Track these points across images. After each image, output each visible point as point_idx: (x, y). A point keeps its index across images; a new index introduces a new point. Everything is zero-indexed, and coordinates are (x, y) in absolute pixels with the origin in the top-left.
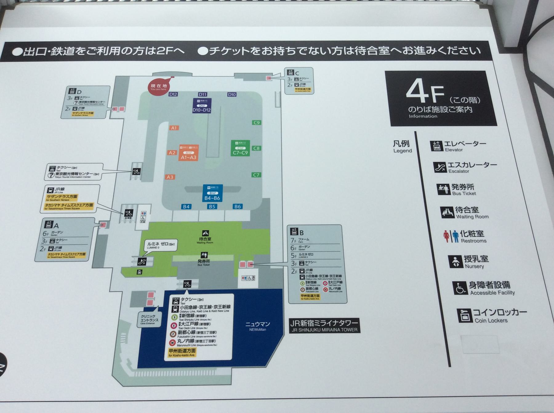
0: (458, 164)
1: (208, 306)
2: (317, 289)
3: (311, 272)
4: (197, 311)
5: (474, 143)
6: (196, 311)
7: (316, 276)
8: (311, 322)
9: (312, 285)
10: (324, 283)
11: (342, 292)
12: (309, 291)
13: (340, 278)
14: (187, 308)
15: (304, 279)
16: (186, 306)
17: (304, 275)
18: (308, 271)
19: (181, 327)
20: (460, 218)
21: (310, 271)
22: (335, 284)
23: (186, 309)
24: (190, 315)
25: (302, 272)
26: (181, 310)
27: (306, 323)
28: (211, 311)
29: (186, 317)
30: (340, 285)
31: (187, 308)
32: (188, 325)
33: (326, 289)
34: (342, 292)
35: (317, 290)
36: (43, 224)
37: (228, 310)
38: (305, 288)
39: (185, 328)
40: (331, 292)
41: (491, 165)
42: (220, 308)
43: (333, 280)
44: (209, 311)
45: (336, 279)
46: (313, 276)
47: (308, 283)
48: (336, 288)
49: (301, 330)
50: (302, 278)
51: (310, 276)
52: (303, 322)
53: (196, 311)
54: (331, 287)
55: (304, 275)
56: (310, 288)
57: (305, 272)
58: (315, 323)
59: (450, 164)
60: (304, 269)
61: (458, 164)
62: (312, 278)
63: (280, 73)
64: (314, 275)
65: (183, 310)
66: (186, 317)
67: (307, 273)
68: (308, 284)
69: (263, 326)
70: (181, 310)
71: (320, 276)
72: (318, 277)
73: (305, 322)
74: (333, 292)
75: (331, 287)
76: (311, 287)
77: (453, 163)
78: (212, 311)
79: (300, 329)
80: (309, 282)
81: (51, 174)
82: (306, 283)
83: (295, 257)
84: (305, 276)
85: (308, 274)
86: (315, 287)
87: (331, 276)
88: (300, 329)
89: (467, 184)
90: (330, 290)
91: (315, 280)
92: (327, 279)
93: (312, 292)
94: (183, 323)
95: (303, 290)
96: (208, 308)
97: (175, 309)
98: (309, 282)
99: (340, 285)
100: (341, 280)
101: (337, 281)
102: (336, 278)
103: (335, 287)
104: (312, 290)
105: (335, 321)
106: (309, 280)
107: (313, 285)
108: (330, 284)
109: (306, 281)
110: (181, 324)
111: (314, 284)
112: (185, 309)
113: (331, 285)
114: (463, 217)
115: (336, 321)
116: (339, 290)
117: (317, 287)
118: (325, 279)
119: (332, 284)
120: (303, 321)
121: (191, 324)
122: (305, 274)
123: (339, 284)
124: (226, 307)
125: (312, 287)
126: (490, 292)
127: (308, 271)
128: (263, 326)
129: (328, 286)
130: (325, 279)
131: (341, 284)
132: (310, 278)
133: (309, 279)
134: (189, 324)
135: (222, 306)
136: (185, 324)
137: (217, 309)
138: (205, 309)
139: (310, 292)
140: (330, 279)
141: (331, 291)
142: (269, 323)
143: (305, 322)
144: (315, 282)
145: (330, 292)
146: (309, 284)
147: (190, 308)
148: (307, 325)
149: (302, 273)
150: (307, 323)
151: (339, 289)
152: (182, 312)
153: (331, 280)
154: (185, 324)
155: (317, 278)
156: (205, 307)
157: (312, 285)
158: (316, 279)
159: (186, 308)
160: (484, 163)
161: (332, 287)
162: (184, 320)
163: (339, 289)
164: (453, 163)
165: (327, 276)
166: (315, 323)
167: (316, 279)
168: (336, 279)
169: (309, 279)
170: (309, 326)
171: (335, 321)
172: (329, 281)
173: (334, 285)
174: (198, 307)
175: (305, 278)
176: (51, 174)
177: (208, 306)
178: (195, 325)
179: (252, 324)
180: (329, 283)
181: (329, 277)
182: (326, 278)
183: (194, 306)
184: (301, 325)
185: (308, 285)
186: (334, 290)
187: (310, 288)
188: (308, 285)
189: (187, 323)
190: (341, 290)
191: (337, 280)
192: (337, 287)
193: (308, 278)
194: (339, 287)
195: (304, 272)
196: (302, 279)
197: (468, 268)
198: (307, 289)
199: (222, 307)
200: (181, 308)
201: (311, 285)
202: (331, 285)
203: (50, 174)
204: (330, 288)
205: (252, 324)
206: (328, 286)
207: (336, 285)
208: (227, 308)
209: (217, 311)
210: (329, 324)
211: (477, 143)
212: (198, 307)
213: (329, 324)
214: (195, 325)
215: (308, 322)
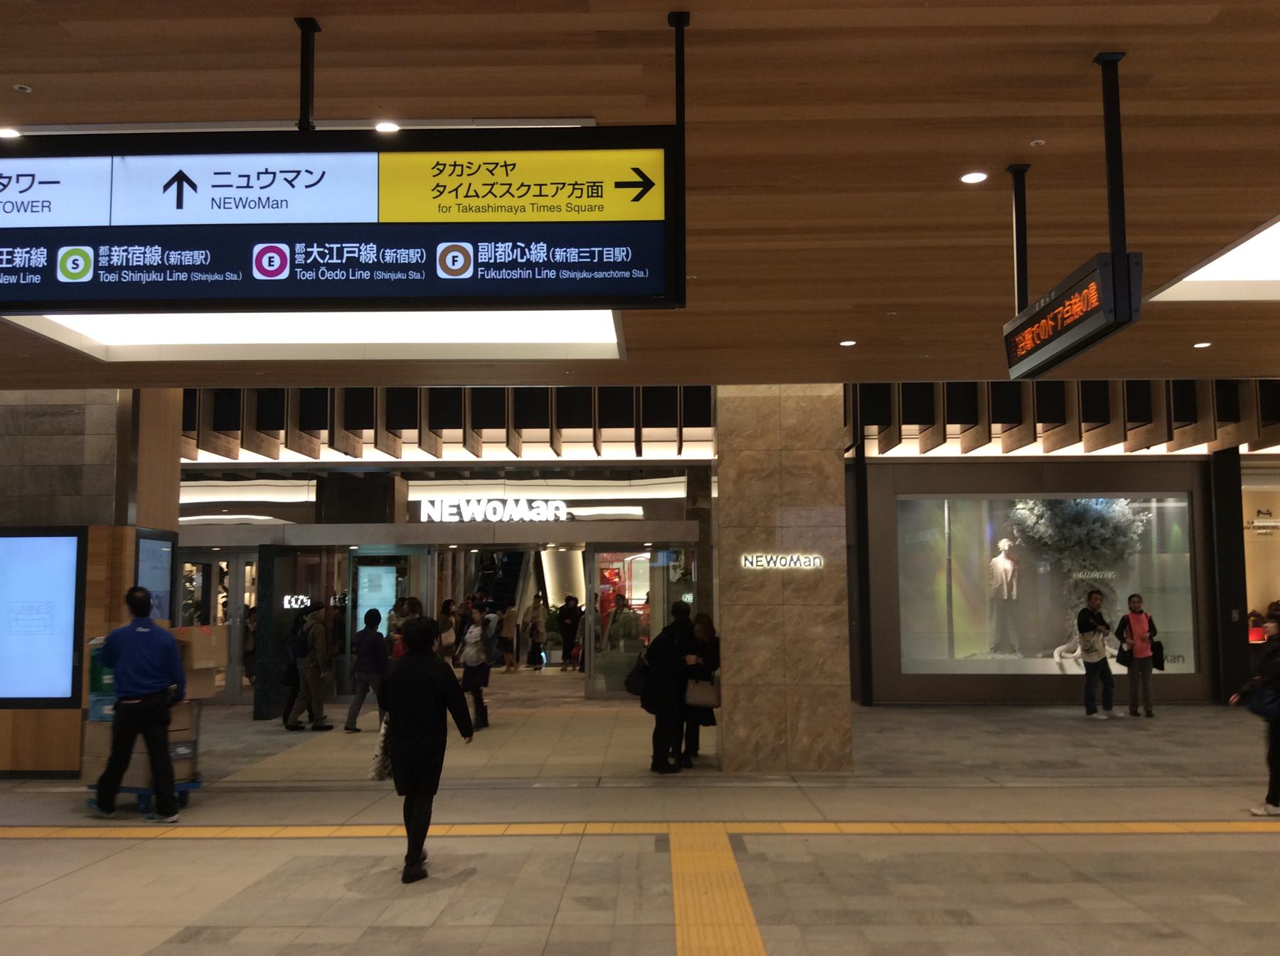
0: (508, 186)
5: (435, 188)
8: (138, 252)
20: (26, 211)
27: (565, 253)
49: (128, 275)
52: (118, 253)
58: (581, 254)
59: (539, 187)
61: (508, 186)
63: (510, 185)
69: (99, 272)
73: (394, 252)
77: (546, 185)
79: (125, 274)
83: (257, 206)
88: (125, 274)
89: (587, 182)
105: (313, 247)
115: (318, 247)
120: (20, 250)
126: (489, 207)
128: (99, 272)
142: (647, 270)
143: (394, 252)
148: (127, 260)
150: (127, 256)
160: (519, 185)
164: (546, 185)
166: (581, 254)
170: (131, 265)
171: (313, 247)
179: (479, 277)
184: (112, 263)
197: (219, 207)
205: (479, 277)
210: (315, 257)
211: (441, 189)
213: (315, 257)
215: (129, 253)
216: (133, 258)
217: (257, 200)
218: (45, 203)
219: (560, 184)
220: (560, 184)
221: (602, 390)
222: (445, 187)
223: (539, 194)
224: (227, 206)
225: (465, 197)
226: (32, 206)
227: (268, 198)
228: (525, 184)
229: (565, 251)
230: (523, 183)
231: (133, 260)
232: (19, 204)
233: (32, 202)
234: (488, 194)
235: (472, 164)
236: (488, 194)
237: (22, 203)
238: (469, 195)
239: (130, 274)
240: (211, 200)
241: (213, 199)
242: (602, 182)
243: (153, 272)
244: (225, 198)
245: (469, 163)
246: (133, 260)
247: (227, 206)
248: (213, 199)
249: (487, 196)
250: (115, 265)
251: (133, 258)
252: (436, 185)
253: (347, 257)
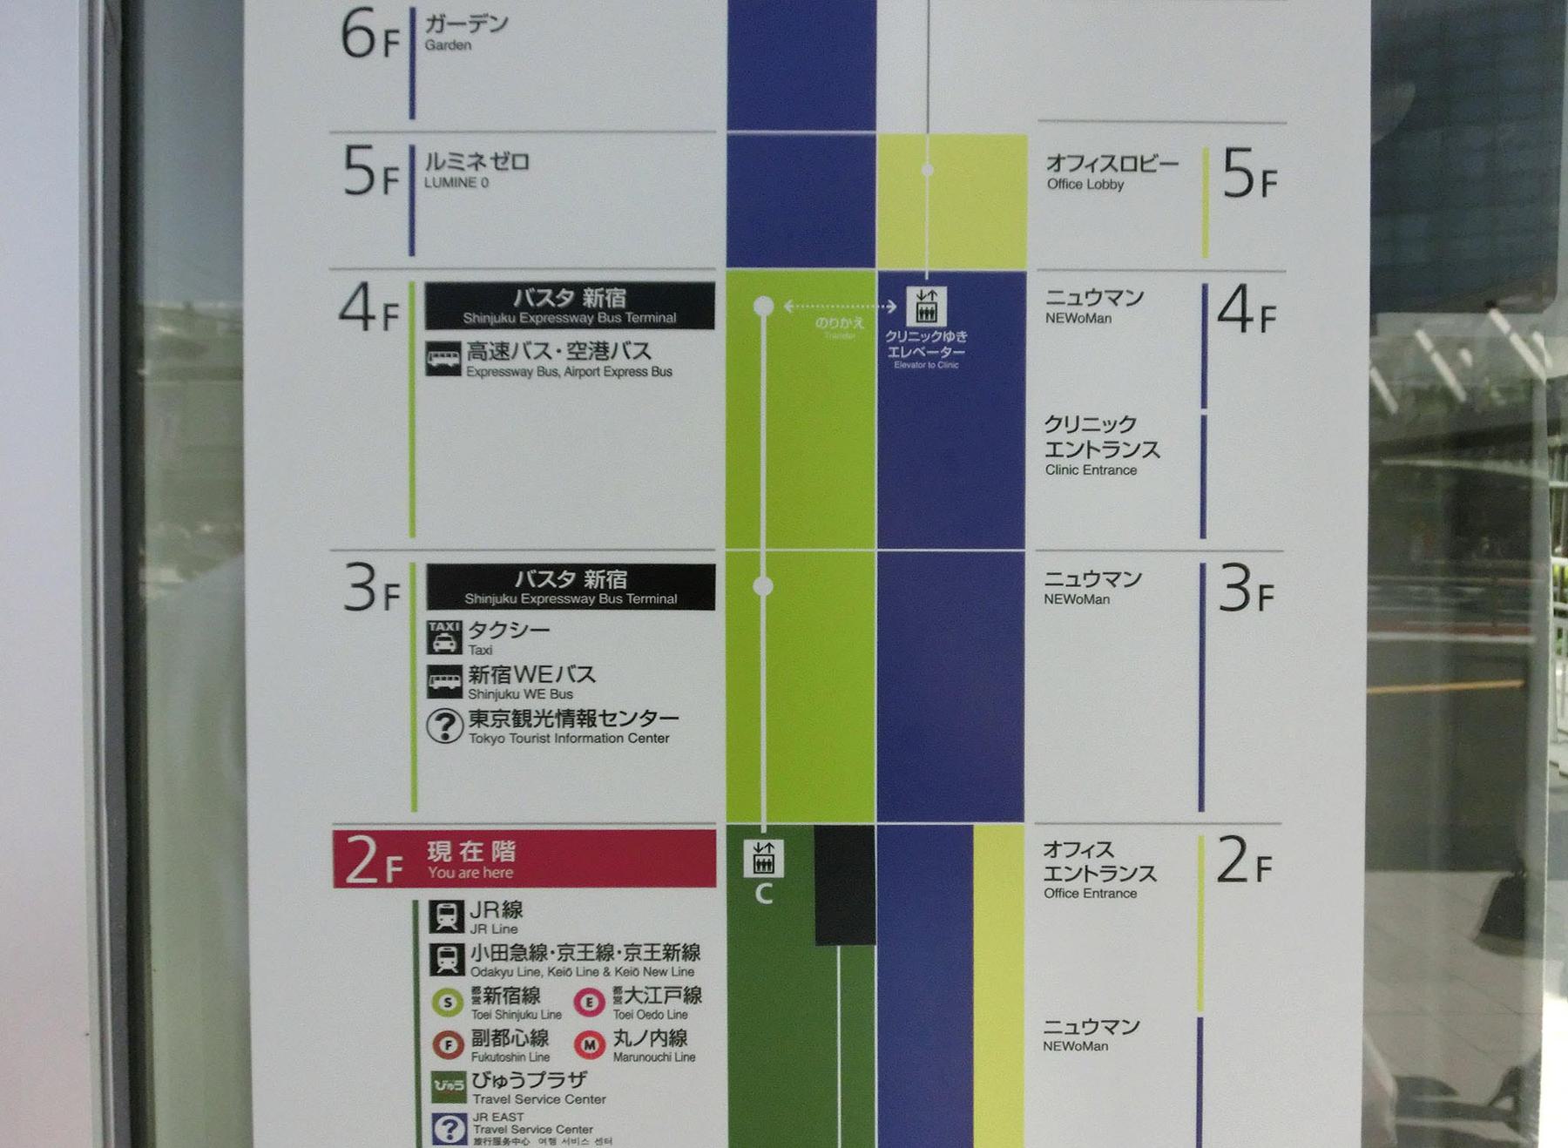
1: (599, 947)
2: (540, 1038)
3: (510, 922)
4: (550, 971)
6: (544, 971)
7: (539, 952)
9: (511, 1015)
10: (583, 1002)
11: (692, 1058)
12: (492, 1050)
13: (688, 965)
14: (503, 956)
15: (461, 969)
16: (500, 945)
17: (461, 947)
18: (492, 914)
19: (624, 1008)
21: (506, 914)
22: (650, 1008)
23: (499, 959)
24: (521, 993)
25: (447, 920)
26: (477, 964)
28: (612, 971)
29: (502, 1000)
30: (684, 1015)
31: (503, 956)
32: (655, 1002)
33: (590, 1039)
34: (692, 1058)
35: (539, 1050)
36: (449, 554)
37: (688, 968)
38: (468, 1038)
39: (641, 1014)
40: (627, 1058)
41: (1084, 430)
42: (652, 959)
43: (641, 982)
44: (602, 971)
45: (664, 973)
46: (518, 952)
47: (488, 999)
48: (659, 1032)
50: (448, 963)
51: (498, 952)
53: (544, 971)
54: (624, 1024)
55: (461, 947)
56: (500, 1036)
57: (469, 923)
60: (461, 904)
62: (512, 965)
64: (527, 946)
65: (486, 963)
66: (502, 1000)
67: (480, 928)
68: (484, 1007)
70: (477, 964)
71: (566, 950)
72: (552, 961)
74: (638, 1058)
75: (624, 1024)
76: (501, 1025)
78: (617, 971)
80: (491, 995)
81: (446, 720)
82: (476, 1000)
84: (468, 952)
85: (487, 940)
86: (528, 1026)
87: (633, 950)
90: (622, 1048)
91: (529, 982)
92: (607, 972)
93: (509, 1058)
94: (634, 992)
95: (448, 1045)
96: (599, 957)
97: (445, 959)
98: (491, 995)
99: (684, 1015)
100: (689, 982)
101: (669, 990)
102: (665, 965)
103: (653, 1025)
104: (512, 1049)
106: (494, 982)
107: (519, 1016)
108: (624, 1008)
109: (476, 989)
110: (626, 996)
111: (523, 1008)
112: (493, 960)
113: (628, 1015)
114: (598, 739)
116: (676, 1048)
117: (538, 1025)
118: (595, 973)
119: (634, 1006)
121: (667, 997)
122: (469, 939)
123: (677, 1004)
124: (681, 954)
125: (510, 1025)
127: (492, 914)
129: (605, 1024)
130: (595, 973)
131: (690, 1008)
132: (501, 965)
133: (494, 973)
134: (661, 995)
135: (661, 948)
136: (642, 997)
137: (637, 964)
138: (586, 959)
139: (498, 1057)
140: (628, 973)
141: (627, 1051)
144: (532, 995)
145: (619, 1057)
146: (495, 1007)
147: (517, 957)
148: (606, 584)
149: (447, 930)
151: (678, 1038)
152: (480, 973)
153: (627, 983)
154: (642, 997)
155: (542, 966)
156: (586, 952)
157: (511, 1015)
158: (536, 973)
159: (496, 956)
160: (1049, 418)
161: (635, 1028)
162: (494, 1015)
163: (678, 1038)
165: (605, 952)
167: (536, 973)
168: (664, 973)
169: (494, 973)
172: (617, 989)
173: (648, 1015)
174: (553, 952)
175: (470, 963)
176: (446, 720)
177: (599, 947)
178: (686, 1000)
180: (618, 1000)
181: (619, 961)
182: (600, 965)
183: (532, 947)
185: (486, 1015)
186: (644, 1047)
187: (497, 1033)
188: (486, 1015)
189: (651, 992)
190: (685, 1050)
191: (669, 981)
192: (667, 1025)
193: (486, 963)
194: (677, 1025)
195: (460, 926)
196: (448, 973)
197: (1052, 602)
198: (479, 1037)
199: (661, 955)
200: (476, 957)
201: (501, 1015)
202: (628, 1015)
203: (439, 718)
204: (621, 1036)
206: (605, 1024)
207: (657, 1015)
208: (685, 957)
209: (641, 970)
212: (553, 952)
214: (686, 1000)
216: (613, 581)
217: (1082, 1044)
218: (489, 905)
219: (1115, 292)
220: (1115, 292)
221: (1024, 553)
222: (655, 714)
223: (1051, 877)
224: (1058, 601)
225: (1222, 878)
226: (541, 674)
227: (1092, 1043)
228: (1055, 417)
229: (605, 574)
230: (1052, 416)
231: (613, 584)
232: (520, 670)
233: (541, 667)
234: (1146, 877)
235: (517, 624)
236: (1146, 877)
237: (525, 668)
238: (1089, 874)
239: (476, 598)
240: (1043, 1044)
241: (1045, 1043)
242: (479, 903)
243: (586, 586)
244: (486, 903)
245: (514, 623)
246: (613, 584)
247: (1058, 601)
248: (1045, 1043)
249: (639, 359)
250: (590, 588)
251: (613, 581)
252: (1124, 417)
253: (548, 584)
